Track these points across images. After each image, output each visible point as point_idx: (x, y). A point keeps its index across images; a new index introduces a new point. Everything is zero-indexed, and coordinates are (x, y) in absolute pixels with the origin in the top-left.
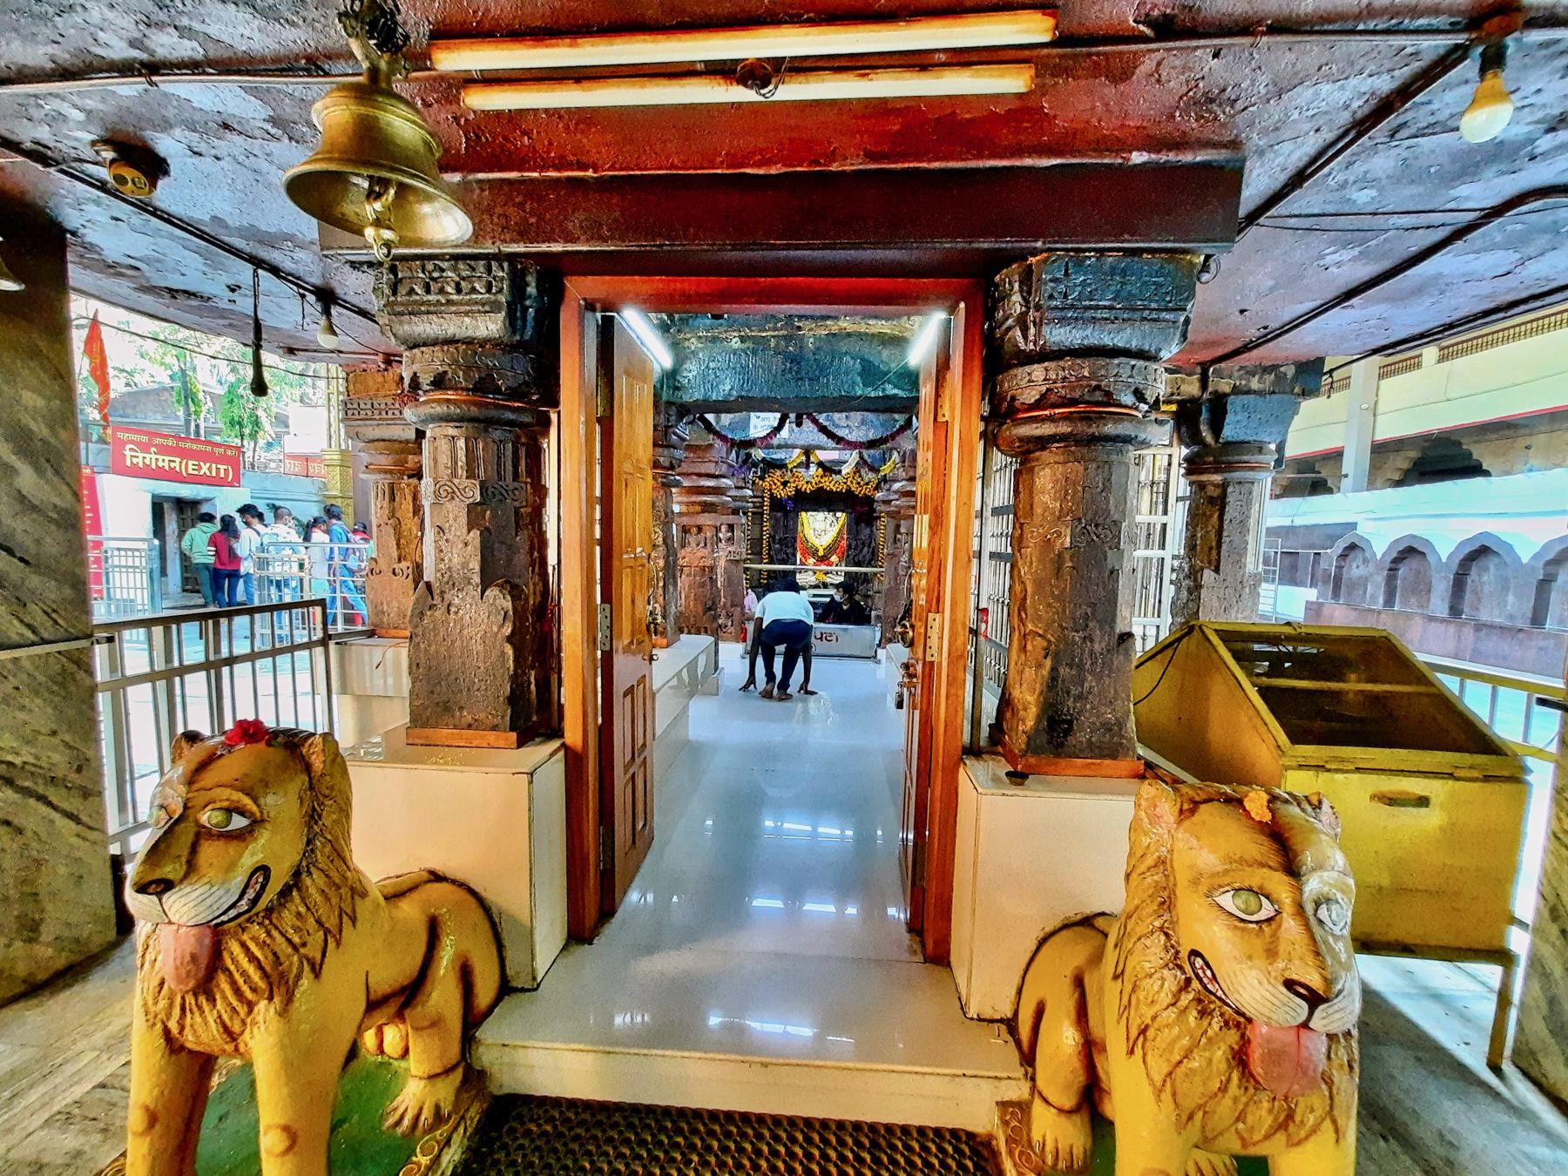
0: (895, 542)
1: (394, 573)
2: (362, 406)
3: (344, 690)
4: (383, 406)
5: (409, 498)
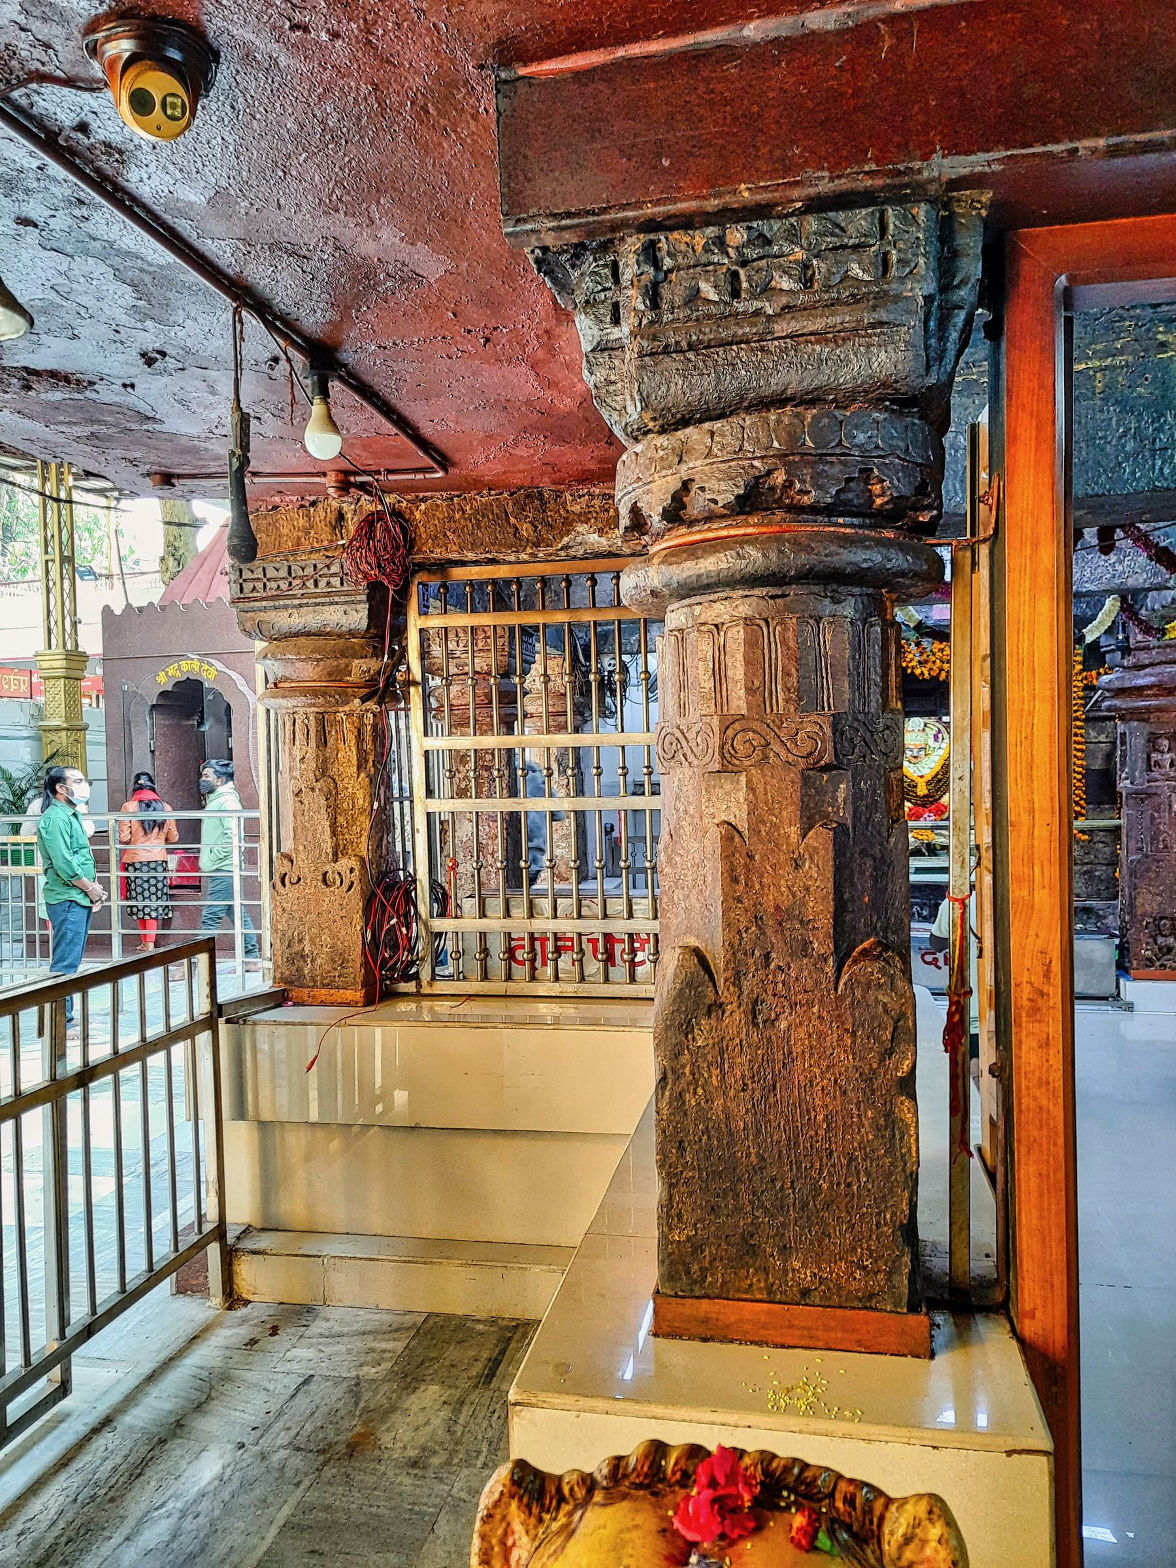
0: (1149, 769)
1: (325, 881)
2: (271, 573)
3: (241, 1114)
4: (309, 571)
5: (351, 738)
